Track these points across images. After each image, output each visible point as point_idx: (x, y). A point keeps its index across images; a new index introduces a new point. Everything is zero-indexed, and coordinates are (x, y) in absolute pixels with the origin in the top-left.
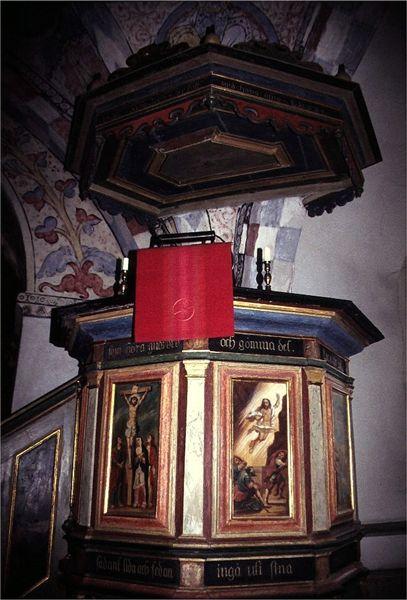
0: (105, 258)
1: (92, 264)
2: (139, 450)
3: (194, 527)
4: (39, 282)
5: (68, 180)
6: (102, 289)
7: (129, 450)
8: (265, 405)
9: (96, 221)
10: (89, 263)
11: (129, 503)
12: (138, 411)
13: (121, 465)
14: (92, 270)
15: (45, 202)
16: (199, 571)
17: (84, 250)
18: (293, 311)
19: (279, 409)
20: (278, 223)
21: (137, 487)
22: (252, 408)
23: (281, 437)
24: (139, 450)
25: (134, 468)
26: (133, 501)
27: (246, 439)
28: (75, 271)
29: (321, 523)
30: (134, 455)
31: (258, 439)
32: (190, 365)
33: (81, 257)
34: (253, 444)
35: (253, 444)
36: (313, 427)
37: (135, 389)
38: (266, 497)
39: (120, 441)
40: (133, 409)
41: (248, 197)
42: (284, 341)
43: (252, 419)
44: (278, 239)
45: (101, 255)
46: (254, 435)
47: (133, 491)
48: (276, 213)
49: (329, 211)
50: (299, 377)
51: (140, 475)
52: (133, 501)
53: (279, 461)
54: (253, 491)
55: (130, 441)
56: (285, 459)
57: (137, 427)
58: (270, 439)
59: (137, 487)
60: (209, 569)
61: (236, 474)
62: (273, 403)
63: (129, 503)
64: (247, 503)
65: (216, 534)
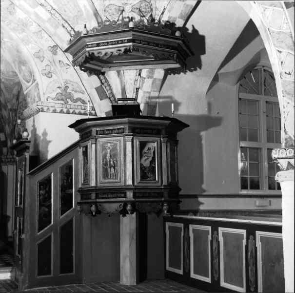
0: (74, 84)
1: (68, 87)
2: (112, 162)
3: (130, 182)
4: (46, 96)
5: (54, 46)
6: (74, 99)
7: (108, 163)
8: (149, 149)
9: (68, 66)
10: (67, 87)
11: (109, 177)
12: (110, 151)
13: (106, 167)
14: (69, 90)
15: (44, 57)
16: (132, 194)
17: (65, 81)
18: (158, 121)
19: (153, 150)
20: (153, 77)
21: (112, 173)
22: (146, 150)
23: (154, 158)
24: (112, 162)
25: (110, 168)
26: (111, 177)
27: (144, 159)
28: (61, 91)
29: (165, 182)
30: (110, 164)
31: (147, 159)
32: (126, 138)
33: (63, 83)
34: (146, 160)
35: (146, 160)
36: (94, 180)
37: (109, 145)
38: (149, 175)
39: (105, 160)
40: (109, 151)
41: (139, 67)
42: (155, 129)
43: (145, 153)
44: (153, 84)
45: (72, 83)
46: (146, 158)
47: (111, 174)
48: (152, 72)
49: (174, 74)
50: (159, 141)
51: (113, 170)
52: (111, 177)
53: (153, 165)
54: (146, 173)
55: (108, 160)
56: (155, 164)
57: (111, 156)
58: (150, 159)
59: (112, 173)
60: (134, 193)
61: (141, 168)
62: (151, 148)
63: (109, 177)
64: (144, 176)
65: (135, 184)
